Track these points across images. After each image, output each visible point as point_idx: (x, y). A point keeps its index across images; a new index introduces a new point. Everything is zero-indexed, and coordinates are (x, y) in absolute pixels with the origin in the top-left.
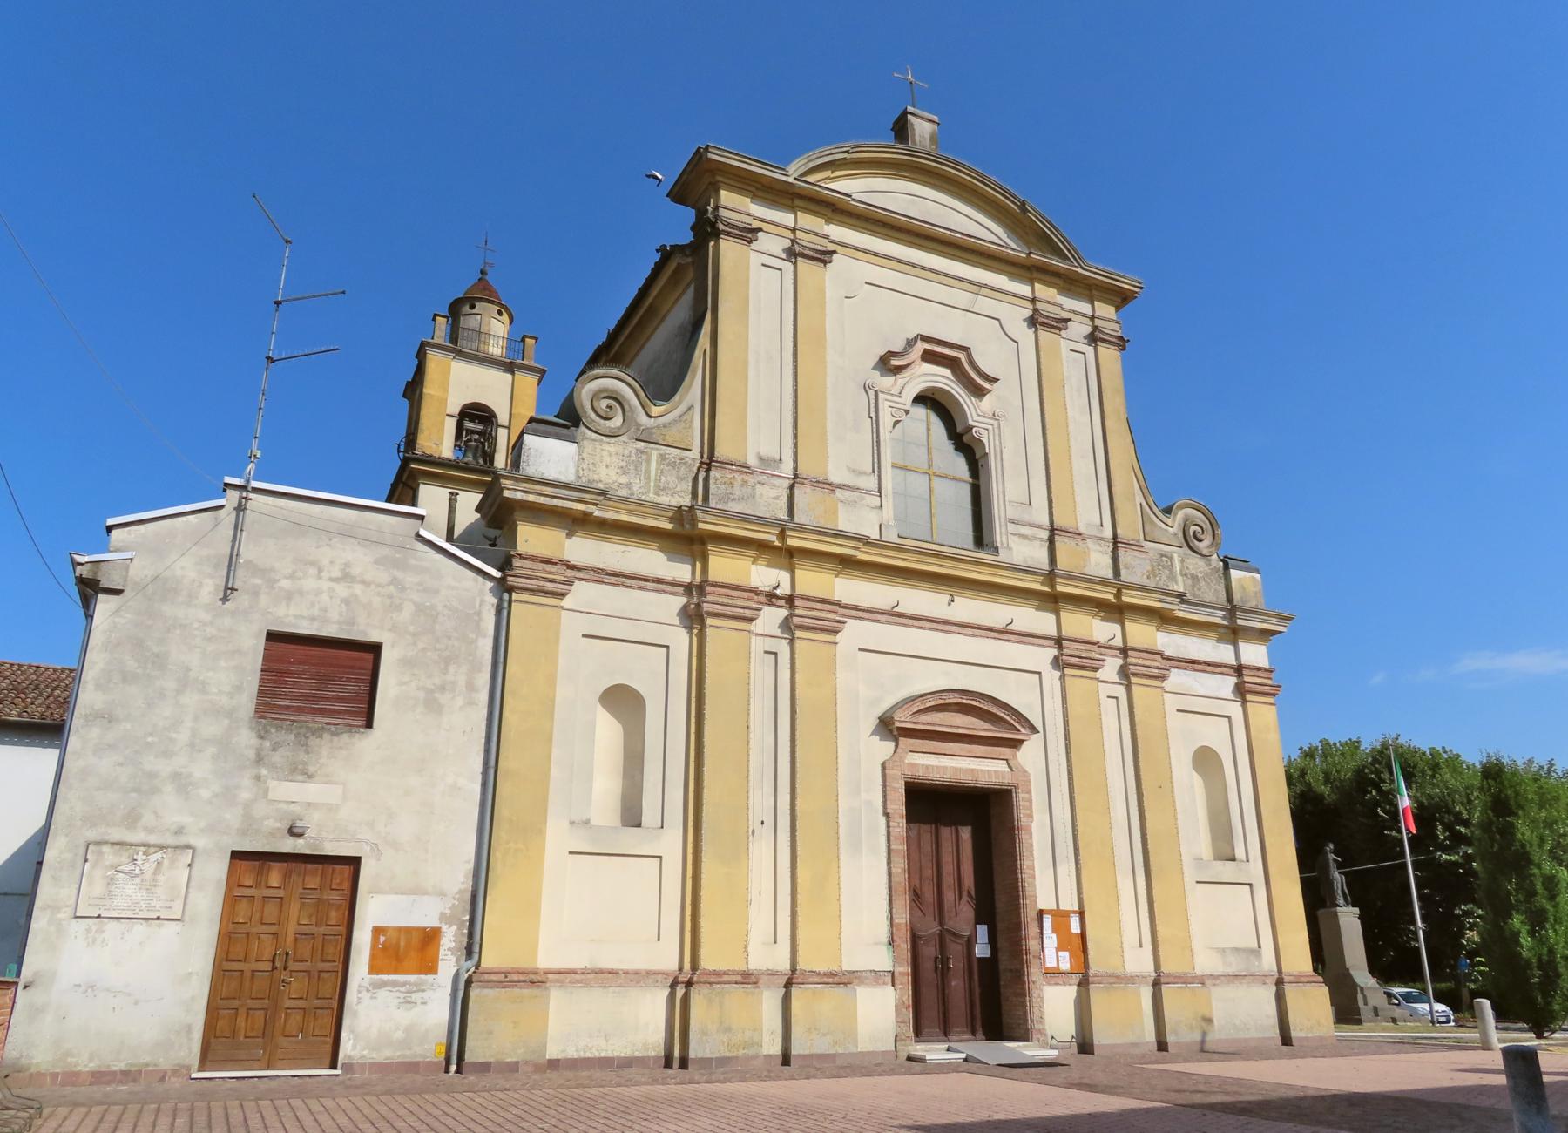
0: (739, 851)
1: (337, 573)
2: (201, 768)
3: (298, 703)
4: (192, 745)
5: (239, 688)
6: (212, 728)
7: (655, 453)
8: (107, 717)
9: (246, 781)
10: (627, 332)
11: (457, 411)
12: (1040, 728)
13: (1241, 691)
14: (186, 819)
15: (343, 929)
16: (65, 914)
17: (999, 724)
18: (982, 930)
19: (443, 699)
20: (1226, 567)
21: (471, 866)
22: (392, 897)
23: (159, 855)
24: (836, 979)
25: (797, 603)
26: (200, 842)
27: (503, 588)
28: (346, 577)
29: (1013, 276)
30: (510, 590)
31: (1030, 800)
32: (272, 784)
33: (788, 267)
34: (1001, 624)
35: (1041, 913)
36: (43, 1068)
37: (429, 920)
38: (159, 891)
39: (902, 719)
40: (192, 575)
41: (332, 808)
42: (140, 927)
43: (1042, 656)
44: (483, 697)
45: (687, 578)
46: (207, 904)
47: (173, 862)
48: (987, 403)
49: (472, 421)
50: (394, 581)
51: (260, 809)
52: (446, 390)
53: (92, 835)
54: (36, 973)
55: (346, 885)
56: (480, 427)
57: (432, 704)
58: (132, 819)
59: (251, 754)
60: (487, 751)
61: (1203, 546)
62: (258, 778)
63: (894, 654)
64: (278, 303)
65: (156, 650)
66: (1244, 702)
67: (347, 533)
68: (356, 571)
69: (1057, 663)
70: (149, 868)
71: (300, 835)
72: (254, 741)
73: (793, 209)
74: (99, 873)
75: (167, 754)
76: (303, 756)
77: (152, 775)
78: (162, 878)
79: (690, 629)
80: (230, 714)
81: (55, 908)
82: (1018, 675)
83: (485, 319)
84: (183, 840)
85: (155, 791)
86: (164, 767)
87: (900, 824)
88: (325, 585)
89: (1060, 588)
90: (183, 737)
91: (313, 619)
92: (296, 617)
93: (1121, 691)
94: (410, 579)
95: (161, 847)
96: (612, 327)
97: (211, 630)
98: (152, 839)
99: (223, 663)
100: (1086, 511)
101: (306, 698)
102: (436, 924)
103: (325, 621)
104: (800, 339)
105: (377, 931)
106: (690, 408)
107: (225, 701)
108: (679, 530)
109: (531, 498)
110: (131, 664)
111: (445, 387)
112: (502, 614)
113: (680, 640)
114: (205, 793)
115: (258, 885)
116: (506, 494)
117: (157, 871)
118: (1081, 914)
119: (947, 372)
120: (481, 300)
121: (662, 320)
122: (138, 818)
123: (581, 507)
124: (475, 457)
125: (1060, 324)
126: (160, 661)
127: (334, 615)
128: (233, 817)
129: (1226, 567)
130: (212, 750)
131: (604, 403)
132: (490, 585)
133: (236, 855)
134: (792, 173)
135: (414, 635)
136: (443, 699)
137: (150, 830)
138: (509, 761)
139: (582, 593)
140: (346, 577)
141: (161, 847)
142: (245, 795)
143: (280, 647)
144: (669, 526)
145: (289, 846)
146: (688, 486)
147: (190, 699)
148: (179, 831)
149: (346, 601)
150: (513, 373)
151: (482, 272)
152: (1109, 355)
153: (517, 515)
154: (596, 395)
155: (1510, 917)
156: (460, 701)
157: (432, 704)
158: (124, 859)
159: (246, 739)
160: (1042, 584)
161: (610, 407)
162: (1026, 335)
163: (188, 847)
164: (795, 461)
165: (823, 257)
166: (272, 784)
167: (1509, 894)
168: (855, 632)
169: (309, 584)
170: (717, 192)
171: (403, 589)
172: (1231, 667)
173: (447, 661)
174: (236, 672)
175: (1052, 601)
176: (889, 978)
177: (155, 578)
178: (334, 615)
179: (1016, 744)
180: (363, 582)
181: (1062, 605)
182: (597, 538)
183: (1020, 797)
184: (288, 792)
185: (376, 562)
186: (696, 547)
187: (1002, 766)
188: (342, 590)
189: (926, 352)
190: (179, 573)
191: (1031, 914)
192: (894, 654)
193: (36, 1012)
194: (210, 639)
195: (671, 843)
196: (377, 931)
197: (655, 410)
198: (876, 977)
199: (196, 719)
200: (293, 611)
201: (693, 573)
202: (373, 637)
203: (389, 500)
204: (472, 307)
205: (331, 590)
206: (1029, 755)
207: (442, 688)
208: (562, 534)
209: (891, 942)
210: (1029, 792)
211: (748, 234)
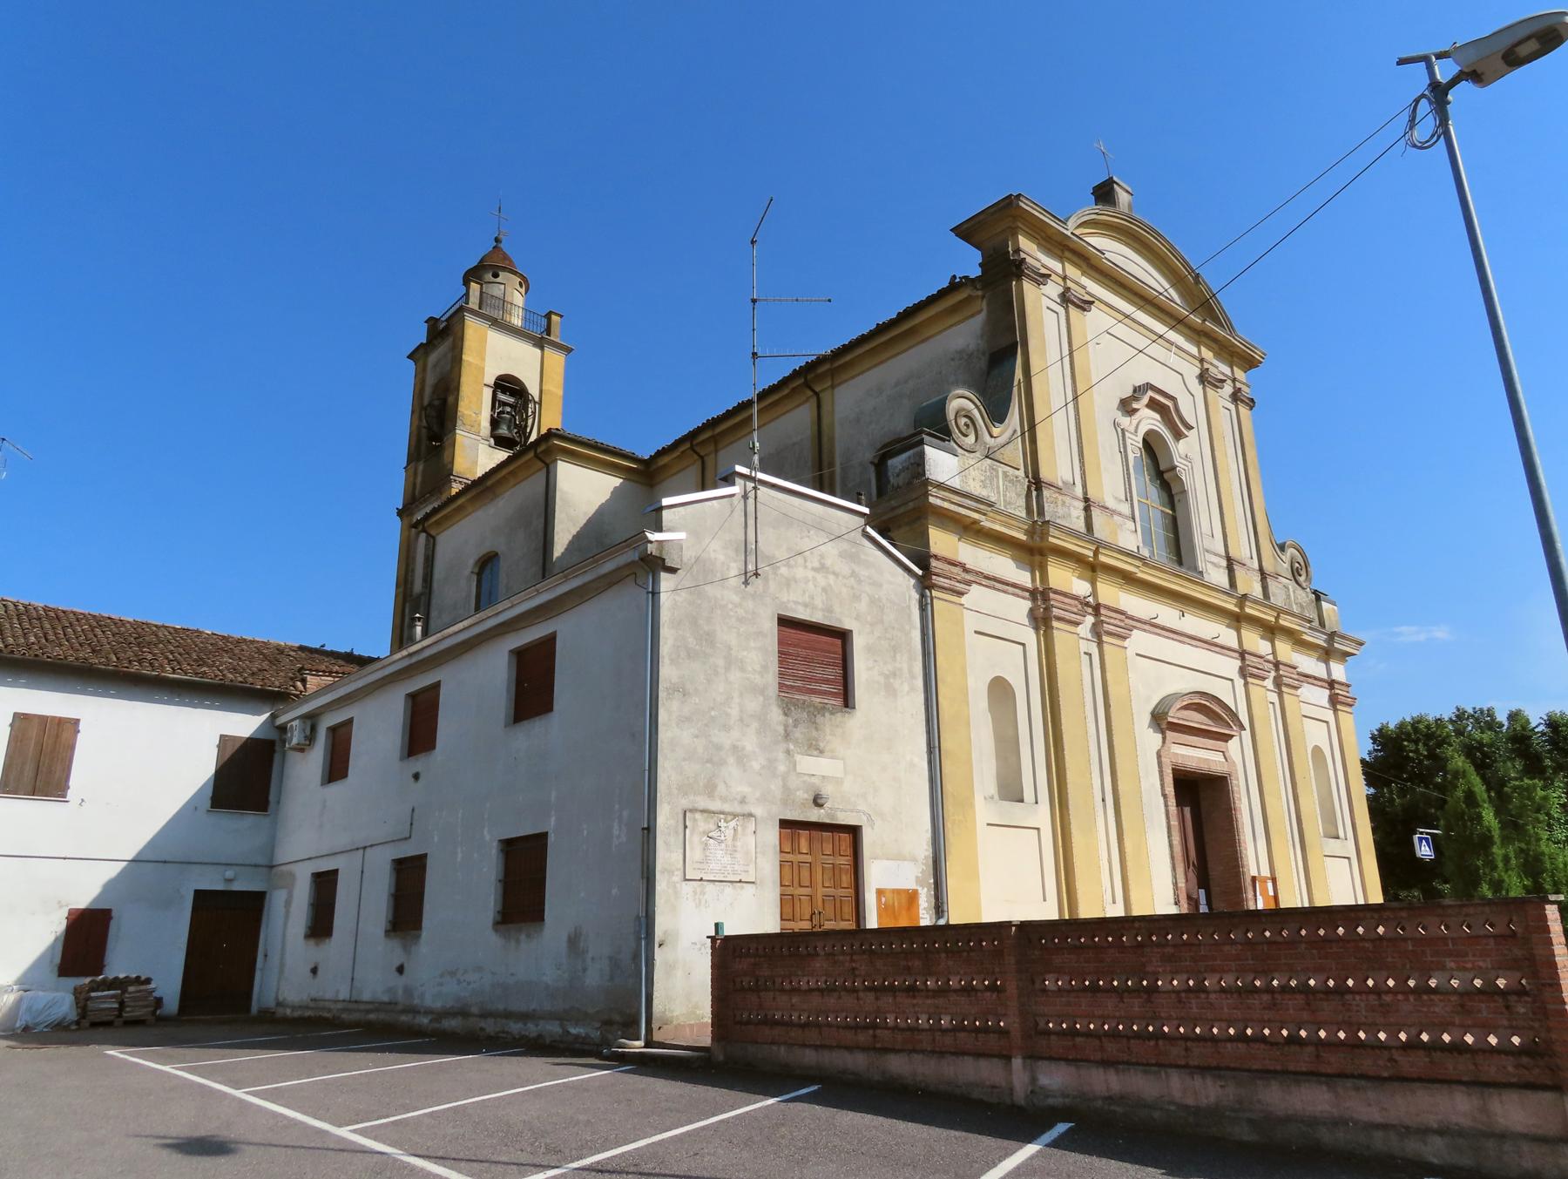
1: (816, 564)
2: (750, 743)
3: (799, 684)
4: (741, 720)
5: (765, 668)
6: (753, 704)
7: (1002, 469)
8: (681, 691)
9: (781, 756)
10: (867, 347)
11: (492, 382)
12: (1246, 723)
13: (1334, 701)
14: (746, 789)
15: (852, 891)
16: (678, 877)
17: (1212, 718)
18: (1202, 891)
19: (896, 683)
20: (1318, 599)
21: (929, 835)
22: (886, 863)
23: (732, 824)
25: (1103, 611)
26: (758, 811)
27: (925, 584)
28: (822, 568)
29: (1188, 338)
30: (931, 587)
32: (798, 757)
34: (1208, 637)
35: (1254, 879)
36: (682, 1020)
37: (909, 884)
38: (738, 855)
39: (1174, 716)
40: (721, 557)
41: (838, 782)
42: (728, 889)
43: (1231, 666)
44: (920, 683)
46: (767, 866)
47: (744, 828)
49: (504, 392)
50: (853, 574)
51: (794, 782)
52: (483, 359)
53: (685, 803)
54: (665, 933)
55: (849, 851)
56: (512, 400)
57: (891, 692)
58: (710, 789)
59: (781, 729)
60: (928, 732)
61: (1302, 579)
62: (788, 752)
63: (1170, 657)
64: (754, 301)
65: (706, 628)
66: (1335, 710)
67: (819, 526)
68: (828, 562)
69: (1243, 672)
70: (729, 833)
71: (821, 806)
72: (782, 718)
73: (1061, 259)
74: (696, 839)
75: (726, 728)
76: (814, 733)
77: (719, 748)
78: (738, 844)
79: (1037, 629)
80: (762, 691)
81: (671, 873)
82: (1218, 676)
83: (509, 289)
84: (747, 809)
85: (723, 763)
86: (725, 739)
87: (1172, 801)
88: (810, 574)
89: (1248, 610)
90: (734, 712)
91: (806, 605)
92: (796, 603)
93: (1274, 697)
94: (864, 573)
95: (735, 816)
97: (741, 612)
98: (727, 807)
99: (752, 644)
100: (1242, 548)
101: (803, 679)
102: (914, 886)
103: (814, 608)
105: (880, 892)
107: (757, 679)
108: (1031, 543)
109: (946, 505)
110: (691, 641)
111: (482, 355)
113: (1029, 636)
114: (756, 765)
115: (792, 852)
116: (931, 499)
117: (735, 838)
118: (1274, 880)
119: (1157, 416)
120: (504, 269)
121: (923, 341)
122: (715, 787)
123: (976, 516)
124: (509, 428)
125: (1218, 383)
126: (709, 639)
127: (818, 602)
128: (775, 787)
129: (1318, 599)
130: (755, 725)
131: (963, 421)
132: (913, 581)
133: (784, 824)
134: (1070, 228)
135: (871, 625)
136: (896, 683)
137: (724, 799)
138: (948, 742)
140: (822, 568)
141: (735, 816)
142: (782, 768)
143: (792, 633)
144: (1024, 538)
145: (815, 815)
146: (1022, 502)
147: (735, 676)
148: (743, 801)
149: (824, 590)
150: (542, 349)
151: (497, 240)
152: (1243, 410)
153: (931, 519)
156: (906, 687)
157: (891, 692)
158: (712, 827)
159: (776, 714)
162: (1197, 388)
163: (751, 815)
164: (1084, 486)
165: (1085, 305)
166: (798, 757)
167: (1478, 868)
168: (1140, 640)
169: (800, 573)
170: (1015, 236)
171: (860, 582)
173: (895, 649)
174: (759, 655)
175: (1237, 620)
177: (697, 559)
178: (818, 602)
179: (1226, 738)
180: (834, 573)
181: (1244, 625)
182: (976, 545)
184: (809, 764)
185: (840, 555)
186: (1037, 558)
187: (1219, 757)
188: (821, 580)
189: (1152, 399)
190: (713, 555)
191: (1248, 881)
192: (1170, 657)
193: (671, 968)
194: (741, 620)
195: (1042, 816)
196: (880, 892)
197: (996, 431)
199: (741, 695)
200: (793, 597)
201: (1033, 580)
202: (847, 624)
203: (703, 488)
204: (495, 275)
205: (814, 579)
207: (894, 675)
208: (955, 538)
211: (1042, 278)
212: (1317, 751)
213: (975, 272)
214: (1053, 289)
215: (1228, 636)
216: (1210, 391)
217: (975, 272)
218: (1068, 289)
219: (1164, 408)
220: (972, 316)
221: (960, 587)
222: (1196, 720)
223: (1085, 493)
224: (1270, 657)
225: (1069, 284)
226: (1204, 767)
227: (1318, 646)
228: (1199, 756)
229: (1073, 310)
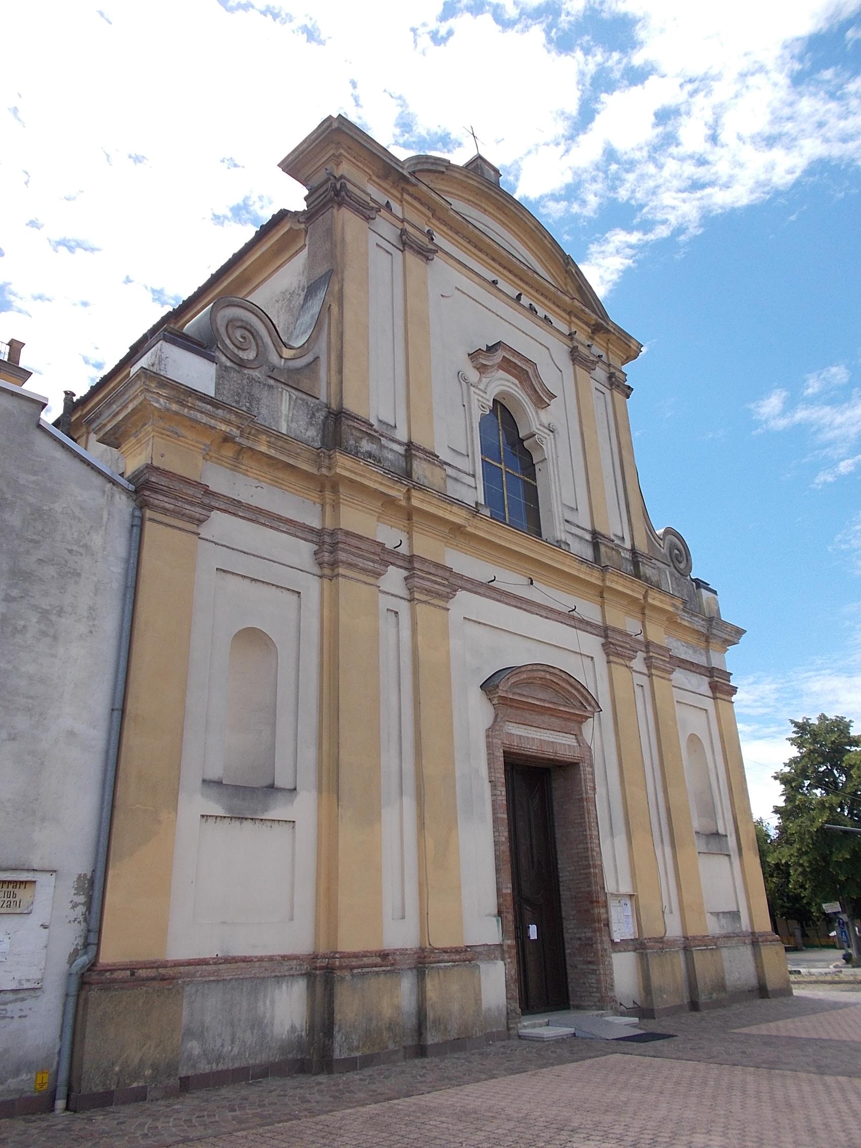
0: (370, 816)
17: (564, 699)
24: (463, 956)
25: (651, 649)
31: (593, 774)
33: (398, 254)
45: (316, 524)
48: (545, 416)
63: (502, 627)
66: (650, 676)
82: (577, 654)
89: (608, 584)
96: (236, 250)
104: (413, 324)
106: (317, 359)
112: (137, 529)
131: (238, 334)
139: (220, 524)
154: (230, 323)
155: (827, 68)
156: (82, 628)
160: (597, 578)
161: (244, 338)
164: (632, 539)
168: (465, 603)
172: (597, 627)
176: (498, 953)
183: (585, 769)
187: (570, 740)
198: (490, 952)
206: (589, 729)
209: (500, 913)
210: (592, 766)
212: (694, 740)
213: (302, 206)
214: (385, 228)
215: (589, 610)
216: (580, 371)
217: (302, 206)
218: (403, 232)
219: (520, 369)
220: (297, 252)
221: (197, 511)
222: (539, 697)
223: (633, 545)
224: (641, 638)
225: (407, 226)
226: (549, 752)
227: (594, 585)
228: (541, 739)
229: (411, 258)
